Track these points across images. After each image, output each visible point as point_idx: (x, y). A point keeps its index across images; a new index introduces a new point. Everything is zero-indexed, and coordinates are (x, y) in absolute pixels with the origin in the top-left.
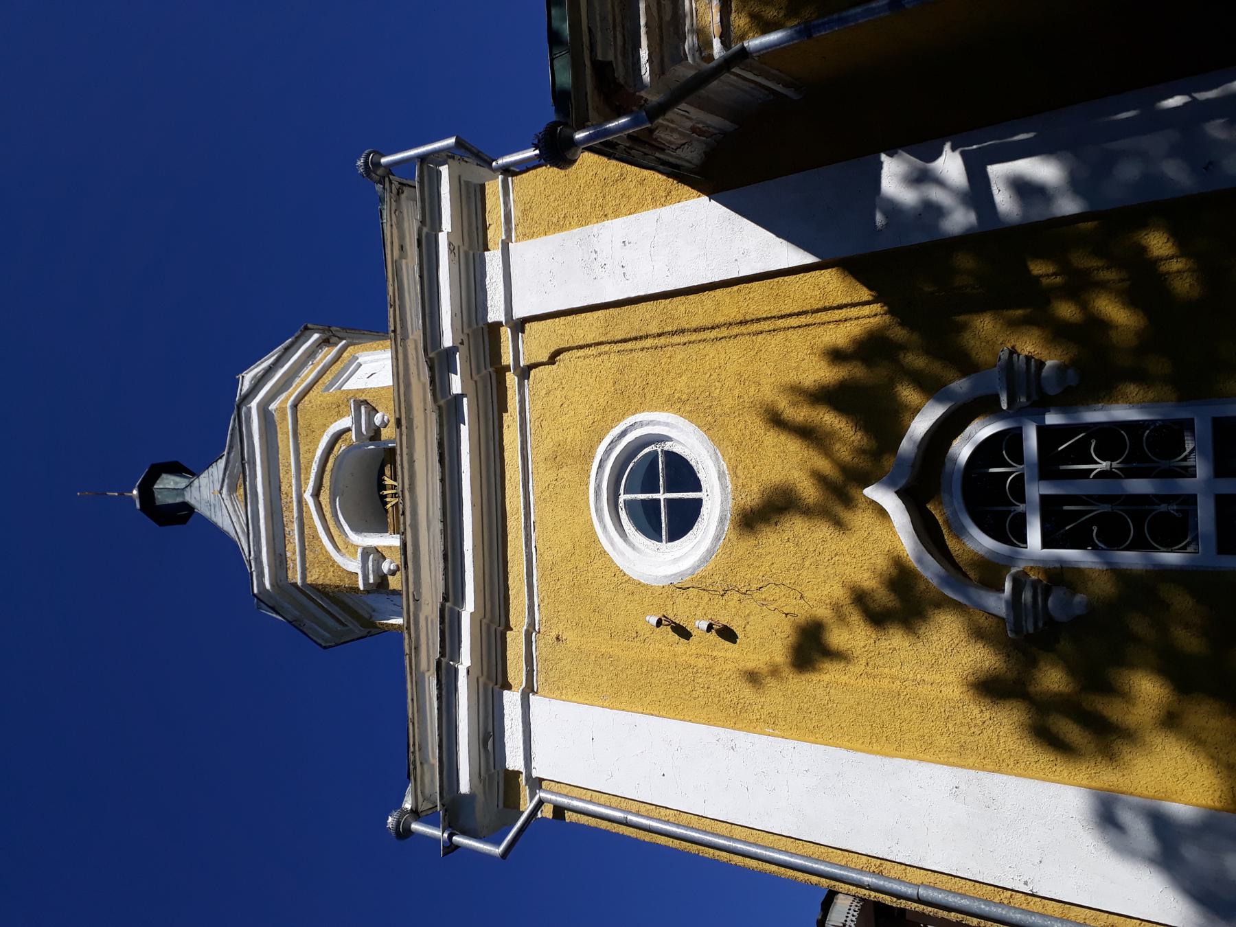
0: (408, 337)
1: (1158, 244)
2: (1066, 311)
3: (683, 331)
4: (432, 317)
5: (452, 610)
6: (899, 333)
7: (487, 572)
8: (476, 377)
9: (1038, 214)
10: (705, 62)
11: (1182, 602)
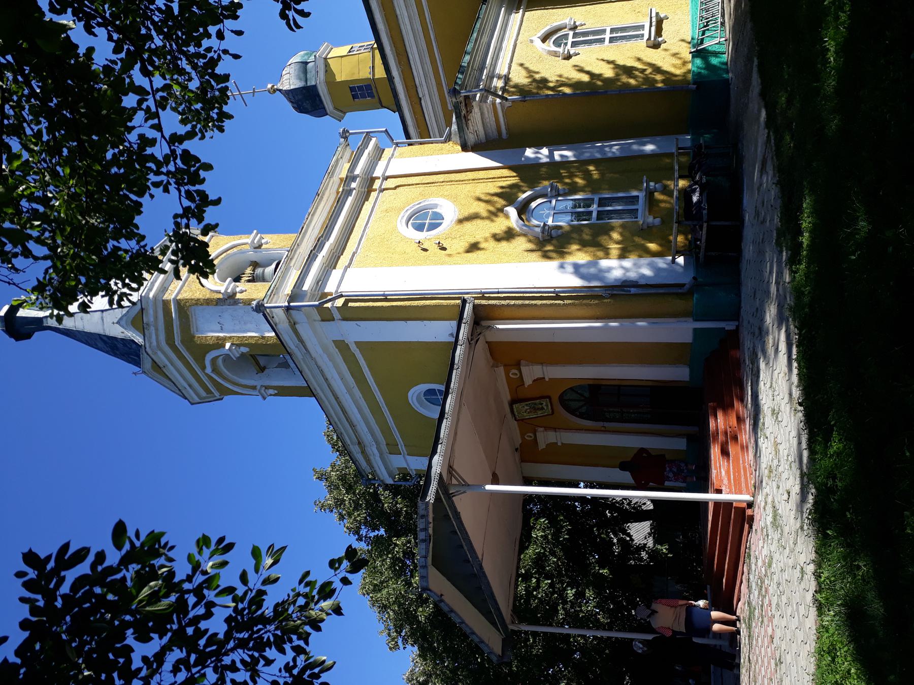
0: (333, 177)
1: (591, 168)
2: (567, 181)
3: (452, 181)
4: (354, 166)
5: (322, 241)
6: (522, 184)
9: (565, 160)
11: (587, 230)
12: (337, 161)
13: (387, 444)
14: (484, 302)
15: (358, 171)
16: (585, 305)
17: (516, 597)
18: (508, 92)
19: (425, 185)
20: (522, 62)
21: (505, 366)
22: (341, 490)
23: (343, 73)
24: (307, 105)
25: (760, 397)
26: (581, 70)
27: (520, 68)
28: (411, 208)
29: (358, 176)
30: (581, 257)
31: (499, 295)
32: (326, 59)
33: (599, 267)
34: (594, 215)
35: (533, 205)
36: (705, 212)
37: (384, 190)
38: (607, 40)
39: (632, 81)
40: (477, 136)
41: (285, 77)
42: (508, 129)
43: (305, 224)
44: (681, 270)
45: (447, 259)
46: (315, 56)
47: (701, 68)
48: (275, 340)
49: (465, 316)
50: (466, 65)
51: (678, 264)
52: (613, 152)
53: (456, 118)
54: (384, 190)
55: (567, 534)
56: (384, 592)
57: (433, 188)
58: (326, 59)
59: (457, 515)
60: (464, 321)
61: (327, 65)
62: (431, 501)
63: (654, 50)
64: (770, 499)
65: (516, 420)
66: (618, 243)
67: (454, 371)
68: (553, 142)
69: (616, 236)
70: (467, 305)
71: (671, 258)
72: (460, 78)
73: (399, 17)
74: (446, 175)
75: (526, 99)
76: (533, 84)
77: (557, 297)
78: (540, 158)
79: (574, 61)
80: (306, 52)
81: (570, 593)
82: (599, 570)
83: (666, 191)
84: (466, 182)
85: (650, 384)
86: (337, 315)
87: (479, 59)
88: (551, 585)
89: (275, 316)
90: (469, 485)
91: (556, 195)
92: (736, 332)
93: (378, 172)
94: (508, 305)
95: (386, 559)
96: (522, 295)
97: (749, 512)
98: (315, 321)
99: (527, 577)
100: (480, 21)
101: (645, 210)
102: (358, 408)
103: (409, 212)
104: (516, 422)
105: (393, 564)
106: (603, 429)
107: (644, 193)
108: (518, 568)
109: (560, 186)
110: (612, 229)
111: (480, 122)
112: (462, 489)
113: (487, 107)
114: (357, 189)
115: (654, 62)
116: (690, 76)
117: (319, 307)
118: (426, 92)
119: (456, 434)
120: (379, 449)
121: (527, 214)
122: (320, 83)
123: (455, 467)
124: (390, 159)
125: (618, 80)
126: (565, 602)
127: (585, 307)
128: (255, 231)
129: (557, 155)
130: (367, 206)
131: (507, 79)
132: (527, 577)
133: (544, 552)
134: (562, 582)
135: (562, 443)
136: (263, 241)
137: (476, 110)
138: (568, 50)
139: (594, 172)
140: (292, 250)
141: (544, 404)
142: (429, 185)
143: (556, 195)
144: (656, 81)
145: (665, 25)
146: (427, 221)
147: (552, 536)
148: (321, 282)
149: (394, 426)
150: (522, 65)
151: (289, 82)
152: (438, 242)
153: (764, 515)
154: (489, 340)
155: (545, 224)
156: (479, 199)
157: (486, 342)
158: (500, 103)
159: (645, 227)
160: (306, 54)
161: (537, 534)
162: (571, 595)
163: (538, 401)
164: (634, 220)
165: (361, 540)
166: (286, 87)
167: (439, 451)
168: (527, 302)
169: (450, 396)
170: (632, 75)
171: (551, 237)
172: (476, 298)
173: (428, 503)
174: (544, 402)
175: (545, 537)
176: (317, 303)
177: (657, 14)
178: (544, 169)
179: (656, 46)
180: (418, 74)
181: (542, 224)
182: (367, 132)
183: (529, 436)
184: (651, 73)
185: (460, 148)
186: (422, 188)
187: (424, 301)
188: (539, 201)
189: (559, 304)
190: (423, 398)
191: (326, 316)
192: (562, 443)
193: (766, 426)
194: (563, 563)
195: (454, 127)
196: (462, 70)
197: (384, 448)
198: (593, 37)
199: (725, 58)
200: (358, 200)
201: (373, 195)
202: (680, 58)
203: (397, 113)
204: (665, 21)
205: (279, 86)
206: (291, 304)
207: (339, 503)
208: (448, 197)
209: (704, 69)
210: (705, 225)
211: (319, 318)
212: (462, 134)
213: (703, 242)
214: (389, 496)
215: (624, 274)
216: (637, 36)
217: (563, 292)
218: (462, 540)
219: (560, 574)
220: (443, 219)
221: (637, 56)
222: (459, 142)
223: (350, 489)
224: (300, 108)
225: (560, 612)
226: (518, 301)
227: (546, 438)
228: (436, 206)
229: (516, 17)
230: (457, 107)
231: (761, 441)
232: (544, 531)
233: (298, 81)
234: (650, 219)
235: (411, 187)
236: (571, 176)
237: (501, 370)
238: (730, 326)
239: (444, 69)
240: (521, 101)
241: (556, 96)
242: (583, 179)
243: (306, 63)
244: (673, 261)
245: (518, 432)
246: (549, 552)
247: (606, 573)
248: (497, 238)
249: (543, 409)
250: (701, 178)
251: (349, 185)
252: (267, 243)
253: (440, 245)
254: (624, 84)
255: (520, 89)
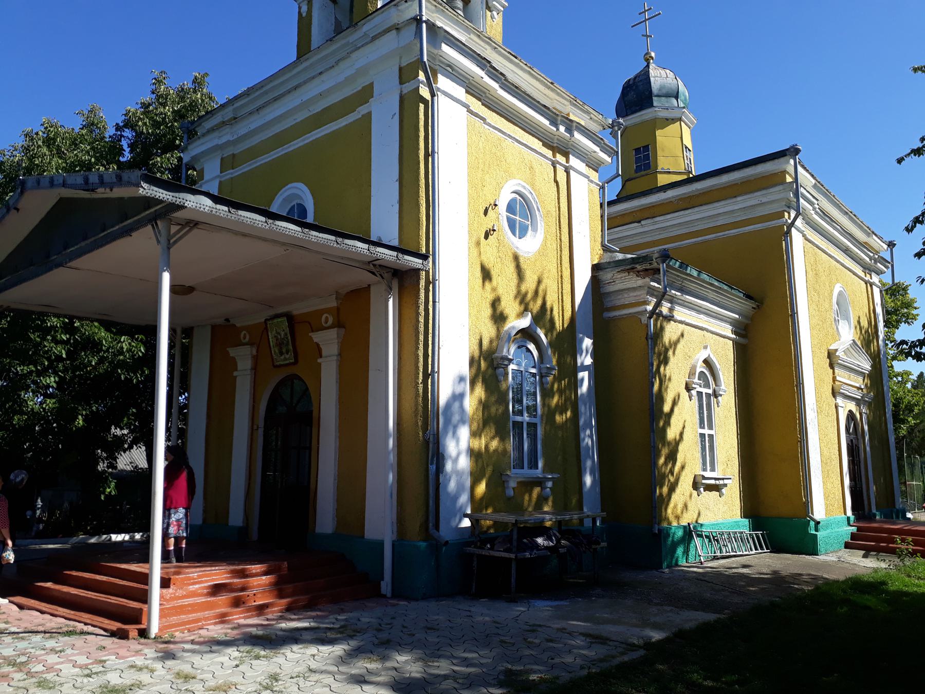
0: (571, 105)
2: (556, 386)
3: (561, 251)
4: (583, 131)
5: (500, 79)
7: (501, 103)
8: (557, 137)
9: (579, 384)
10: (299, 195)
12: (588, 113)
13: (234, 155)
14: (422, 283)
15: (577, 135)
16: (417, 409)
17: (43, 315)
18: (656, 320)
19: (558, 218)
20: (685, 336)
21: (338, 309)
22: (179, 104)
23: (665, 138)
24: (632, 95)
25: (295, 648)
26: (675, 403)
27: (680, 334)
28: (534, 199)
29: (572, 135)
30: (470, 404)
31: (431, 303)
32: (680, 120)
33: (459, 425)
34: (519, 418)
35: (532, 347)
36: (527, 555)
37: (555, 167)
38: (702, 431)
39: (662, 461)
40: (608, 283)
41: (663, 72)
42: (614, 319)
43: (520, 61)
44: (453, 524)
45: (474, 239)
46: (684, 108)
47: (673, 537)
48: (371, 9)
49: (407, 257)
50: (688, 272)
51: (460, 521)
52: (584, 439)
53: (632, 258)
54: (555, 167)
55: (126, 378)
56: (45, 150)
57: (554, 228)
58: (680, 120)
59: (127, 232)
60: (400, 255)
61: (673, 120)
62: (141, 190)
63: (691, 484)
64: (145, 677)
65: (266, 320)
66: (487, 447)
67: (333, 238)
68: (597, 371)
69: (494, 444)
70: (420, 261)
71: (469, 512)
72: (675, 263)
73: (734, 200)
74: (568, 245)
75: (650, 341)
76: (663, 349)
77: (426, 376)
78: (581, 355)
79: (684, 394)
80: (688, 98)
81: (52, 380)
82: (82, 415)
83: (542, 499)
84: (559, 269)
85: (312, 486)
86: (408, 87)
87: (692, 286)
88: (59, 358)
89: (407, 4)
90: (169, 248)
91: (541, 373)
92: (374, 593)
93: (574, 162)
94: (418, 314)
95: (89, 155)
96: (430, 331)
97: (133, 630)
98: (401, 58)
99: (69, 328)
100: (729, 290)
101: (525, 478)
102: (281, 116)
103: (529, 196)
104: (263, 320)
105: (82, 164)
106: (255, 427)
107: (540, 476)
108: (80, 319)
109: (550, 378)
110: (503, 439)
111: (625, 287)
112: (163, 239)
113: (641, 295)
114: (557, 133)
115: (680, 484)
116: (665, 525)
117: (419, 64)
118: (646, 229)
119: (244, 235)
120: (228, 143)
121: (521, 339)
122: (655, 111)
123: (195, 231)
124: (587, 177)
125: (664, 445)
126: (40, 374)
127: (413, 410)
128: (507, 4)
129: (584, 375)
130: (537, 144)
131: (670, 318)
132: (69, 328)
133: (103, 350)
134: (65, 370)
135: (236, 377)
136: (495, 13)
137: (640, 282)
138: (695, 388)
139: (564, 418)
140: (489, 40)
141: (287, 356)
142: (558, 224)
143: (541, 373)
144: (661, 487)
145: (715, 494)
146: (518, 218)
147: (122, 360)
148: (450, 70)
149: (258, 164)
150: (682, 335)
151: (658, 77)
152: (495, 228)
153: (121, 667)
154: (372, 288)
155: (510, 361)
156: (539, 282)
157: (369, 285)
158: (646, 310)
159: (504, 478)
160: (685, 99)
161: (125, 342)
162: (48, 382)
163: (291, 347)
164: (512, 464)
165: (117, 130)
166: (652, 72)
167: (219, 207)
168: (421, 337)
169: (299, 229)
170: (668, 460)
171: (496, 368)
172: (427, 272)
173: (138, 185)
174: (289, 357)
175: (121, 352)
176: (425, 59)
177: (725, 485)
178: (569, 359)
179: (695, 485)
180: (668, 220)
181: (510, 357)
182: (617, 152)
183: (245, 336)
184: (669, 480)
185: (595, 262)
186: (555, 214)
187: (424, 205)
188: (535, 353)
189: (418, 378)
190: (294, 203)
191: (406, 74)
192: (236, 377)
193: (255, 662)
194: (90, 373)
195: (620, 256)
196: (683, 265)
197: (228, 152)
198: (706, 418)
199: (682, 562)
200: (544, 134)
201: (549, 153)
202: (682, 513)
203: (616, 198)
204: (718, 493)
205: (652, 66)
206: (424, 25)
207: (162, 100)
208: (545, 239)
209: (673, 540)
210: (513, 556)
211: (404, 64)
212: (612, 265)
213: (490, 551)
214: (171, 164)
215: (450, 457)
216: (704, 463)
217: (433, 383)
218: (93, 239)
219: (75, 369)
220: (520, 238)
221: (687, 464)
222: (602, 261)
223: (179, 115)
224: (628, 88)
225: (25, 368)
226: (422, 326)
227: (243, 357)
228: (535, 230)
229: (727, 330)
230: (645, 259)
231: (233, 652)
232: (129, 351)
233: (658, 87)
234: (513, 484)
235: (557, 200)
236: (561, 392)
237: (333, 304)
238: (386, 586)
239: (695, 244)
240: (647, 334)
241: (651, 375)
242: (557, 405)
243: (677, 97)
244: (466, 516)
245: (250, 323)
246: (103, 356)
247: (79, 423)
248: (495, 303)
249: (281, 353)
250: (563, 547)
251: (563, 123)
252: (492, 17)
253: (492, 232)
254: (660, 451)
255: (660, 332)
